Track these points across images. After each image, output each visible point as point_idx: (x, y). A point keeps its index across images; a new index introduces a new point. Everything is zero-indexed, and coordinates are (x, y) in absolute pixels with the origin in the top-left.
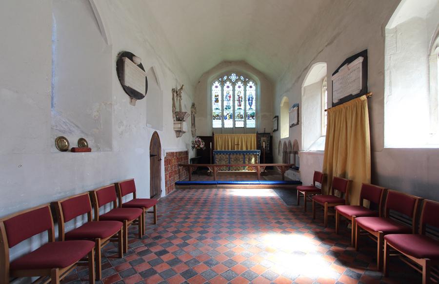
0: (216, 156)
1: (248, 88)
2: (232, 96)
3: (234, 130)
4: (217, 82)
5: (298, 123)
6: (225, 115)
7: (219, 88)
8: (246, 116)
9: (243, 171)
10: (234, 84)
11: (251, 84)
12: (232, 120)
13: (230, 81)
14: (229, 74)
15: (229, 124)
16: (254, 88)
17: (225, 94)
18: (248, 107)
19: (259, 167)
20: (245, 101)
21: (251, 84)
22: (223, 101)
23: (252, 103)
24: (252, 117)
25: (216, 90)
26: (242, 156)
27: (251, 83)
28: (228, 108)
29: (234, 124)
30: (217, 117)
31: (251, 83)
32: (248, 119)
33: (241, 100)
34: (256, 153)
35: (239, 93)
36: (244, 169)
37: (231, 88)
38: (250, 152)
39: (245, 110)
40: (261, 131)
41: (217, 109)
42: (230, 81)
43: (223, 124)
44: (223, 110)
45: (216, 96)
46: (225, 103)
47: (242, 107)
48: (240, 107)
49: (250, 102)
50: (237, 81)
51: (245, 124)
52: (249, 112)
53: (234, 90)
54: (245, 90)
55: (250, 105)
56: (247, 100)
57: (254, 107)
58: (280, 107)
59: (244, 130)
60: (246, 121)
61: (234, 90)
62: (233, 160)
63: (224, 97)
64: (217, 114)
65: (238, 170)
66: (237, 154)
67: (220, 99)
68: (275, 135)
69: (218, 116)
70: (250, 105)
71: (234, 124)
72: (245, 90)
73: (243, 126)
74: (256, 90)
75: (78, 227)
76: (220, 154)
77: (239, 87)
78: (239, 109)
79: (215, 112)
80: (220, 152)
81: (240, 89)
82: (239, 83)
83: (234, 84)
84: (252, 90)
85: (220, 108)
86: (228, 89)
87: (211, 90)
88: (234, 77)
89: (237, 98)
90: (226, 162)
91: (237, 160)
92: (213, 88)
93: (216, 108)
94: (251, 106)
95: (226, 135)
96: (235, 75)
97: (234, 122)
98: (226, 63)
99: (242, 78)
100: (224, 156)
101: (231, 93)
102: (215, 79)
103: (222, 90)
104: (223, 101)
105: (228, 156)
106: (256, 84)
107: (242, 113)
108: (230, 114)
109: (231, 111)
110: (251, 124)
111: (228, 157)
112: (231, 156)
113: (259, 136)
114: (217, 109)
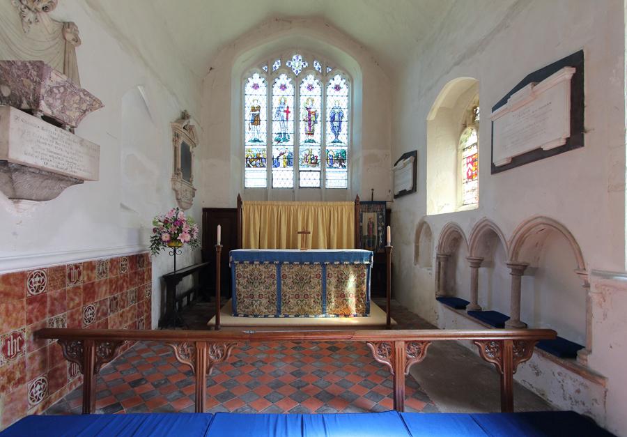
0: (239, 269)
1: (330, 90)
2: (291, 110)
3: (298, 193)
4: (256, 76)
5: (414, 189)
6: (275, 157)
7: (263, 90)
8: (324, 161)
9: (321, 319)
10: (297, 80)
11: (338, 80)
12: (291, 168)
13: (289, 71)
14: (284, 54)
15: (283, 178)
16: (345, 90)
17: (276, 104)
18: (330, 137)
19: (400, 345)
20: (324, 122)
21: (338, 80)
22: (270, 121)
23: (340, 127)
24: (341, 161)
25: (254, 94)
26: (318, 269)
27: (338, 77)
28: (283, 138)
29: (297, 179)
30: (257, 161)
31: (338, 77)
32: (331, 167)
33: (313, 119)
34: (362, 260)
35: (310, 103)
36: (323, 311)
37: (290, 89)
38: (340, 257)
39: (323, 144)
40: (365, 197)
41: (255, 141)
42: (289, 71)
43: (270, 179)
44: (270, 144)
45: (253, 109)
46: (276, 128)
47: (317, 137)
48: (310, 137)
49: (336, 124)
50: (305, 72)
51: (323, 179)
52: (334, 150)
53: (297, 95)
54: (324, 96)
55: (336, 131)
56: (328, 119)
57: (343, 137)
58: (426, 122)
59: (321, 193)
60: (324, 171)
61: (297, 95)
62: (289, 281)
63: (274, 111)
64: (255, 152)
65: (307, 316)
66: (302, 263)
67: (263, 115)
68: (401, 208)
69: (258, 158)
70: (336, 131)
71: (297, 179)
72: (324, 96)
73: (318, 185)
74: (351, 96)
75: (531, 84)
76: (252, 263)
77: (310, 88)
78: (309, 141)
79: (252, 149)
80: (252, 258)
81: (311, 94)
82: (310, 79)
83: (297, 80)
84: (339, 97)
85: (264, 138)
86: (283, 93)
87: (242, 95)
88: (297, 63)
89: (303, 114)
90: (267, 288)
91: (301, 281)
92: (249, 89)
93: (253, 138)
94: (337, 134)
95: (275, 203)
96: (300, 58)
97: (297, 172)
98: (279, 20)
99: (317, 66)
100: (262, 268)
101: (290, 102)
102: (252, 66)
103: (270, 95)
104: (270, 121)
105: (273, 269)
106: (350, 80)
107: (316, 152)
108: (286, 155)
109: (289, 147)
110: (337, 178)
111: (275, 271)
112: (286, 269)
113: (361, 206)
114: (255, 141)
